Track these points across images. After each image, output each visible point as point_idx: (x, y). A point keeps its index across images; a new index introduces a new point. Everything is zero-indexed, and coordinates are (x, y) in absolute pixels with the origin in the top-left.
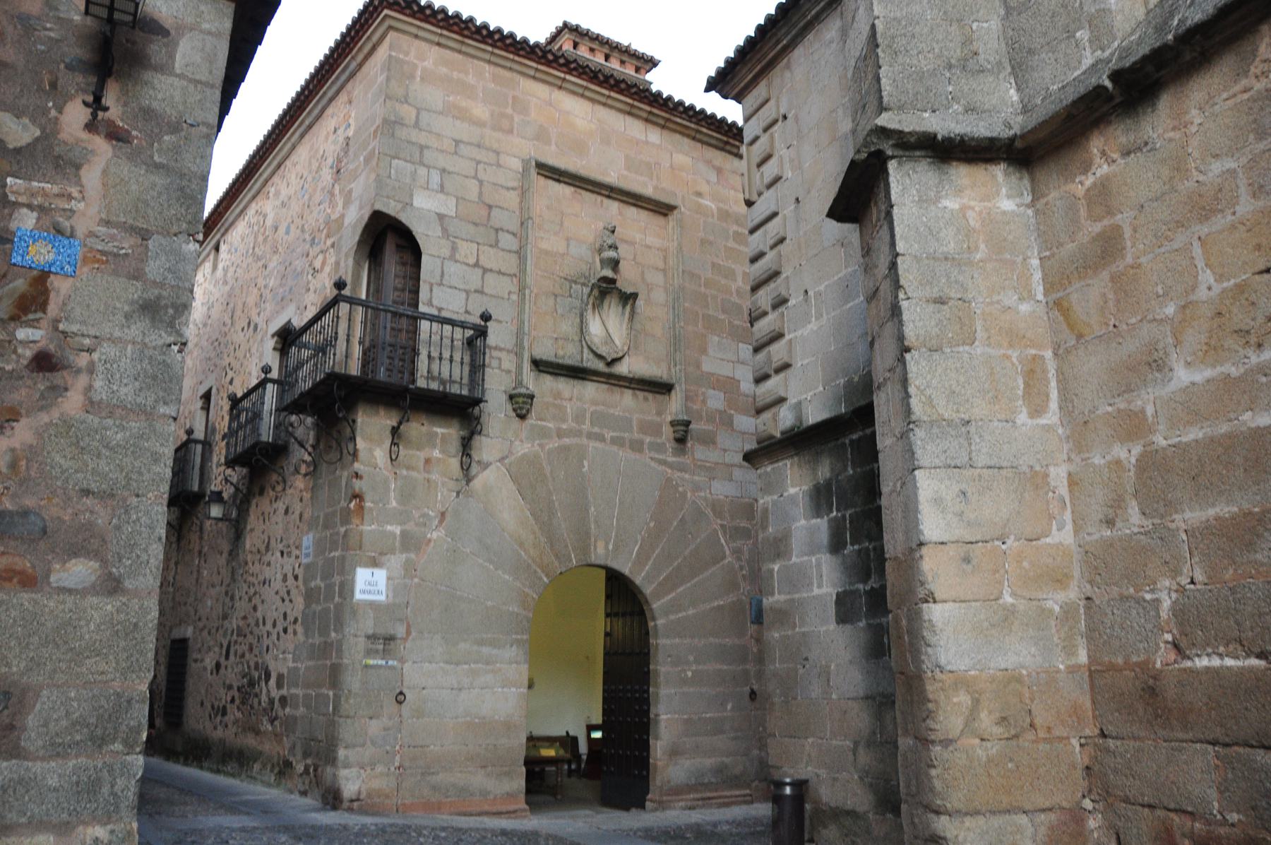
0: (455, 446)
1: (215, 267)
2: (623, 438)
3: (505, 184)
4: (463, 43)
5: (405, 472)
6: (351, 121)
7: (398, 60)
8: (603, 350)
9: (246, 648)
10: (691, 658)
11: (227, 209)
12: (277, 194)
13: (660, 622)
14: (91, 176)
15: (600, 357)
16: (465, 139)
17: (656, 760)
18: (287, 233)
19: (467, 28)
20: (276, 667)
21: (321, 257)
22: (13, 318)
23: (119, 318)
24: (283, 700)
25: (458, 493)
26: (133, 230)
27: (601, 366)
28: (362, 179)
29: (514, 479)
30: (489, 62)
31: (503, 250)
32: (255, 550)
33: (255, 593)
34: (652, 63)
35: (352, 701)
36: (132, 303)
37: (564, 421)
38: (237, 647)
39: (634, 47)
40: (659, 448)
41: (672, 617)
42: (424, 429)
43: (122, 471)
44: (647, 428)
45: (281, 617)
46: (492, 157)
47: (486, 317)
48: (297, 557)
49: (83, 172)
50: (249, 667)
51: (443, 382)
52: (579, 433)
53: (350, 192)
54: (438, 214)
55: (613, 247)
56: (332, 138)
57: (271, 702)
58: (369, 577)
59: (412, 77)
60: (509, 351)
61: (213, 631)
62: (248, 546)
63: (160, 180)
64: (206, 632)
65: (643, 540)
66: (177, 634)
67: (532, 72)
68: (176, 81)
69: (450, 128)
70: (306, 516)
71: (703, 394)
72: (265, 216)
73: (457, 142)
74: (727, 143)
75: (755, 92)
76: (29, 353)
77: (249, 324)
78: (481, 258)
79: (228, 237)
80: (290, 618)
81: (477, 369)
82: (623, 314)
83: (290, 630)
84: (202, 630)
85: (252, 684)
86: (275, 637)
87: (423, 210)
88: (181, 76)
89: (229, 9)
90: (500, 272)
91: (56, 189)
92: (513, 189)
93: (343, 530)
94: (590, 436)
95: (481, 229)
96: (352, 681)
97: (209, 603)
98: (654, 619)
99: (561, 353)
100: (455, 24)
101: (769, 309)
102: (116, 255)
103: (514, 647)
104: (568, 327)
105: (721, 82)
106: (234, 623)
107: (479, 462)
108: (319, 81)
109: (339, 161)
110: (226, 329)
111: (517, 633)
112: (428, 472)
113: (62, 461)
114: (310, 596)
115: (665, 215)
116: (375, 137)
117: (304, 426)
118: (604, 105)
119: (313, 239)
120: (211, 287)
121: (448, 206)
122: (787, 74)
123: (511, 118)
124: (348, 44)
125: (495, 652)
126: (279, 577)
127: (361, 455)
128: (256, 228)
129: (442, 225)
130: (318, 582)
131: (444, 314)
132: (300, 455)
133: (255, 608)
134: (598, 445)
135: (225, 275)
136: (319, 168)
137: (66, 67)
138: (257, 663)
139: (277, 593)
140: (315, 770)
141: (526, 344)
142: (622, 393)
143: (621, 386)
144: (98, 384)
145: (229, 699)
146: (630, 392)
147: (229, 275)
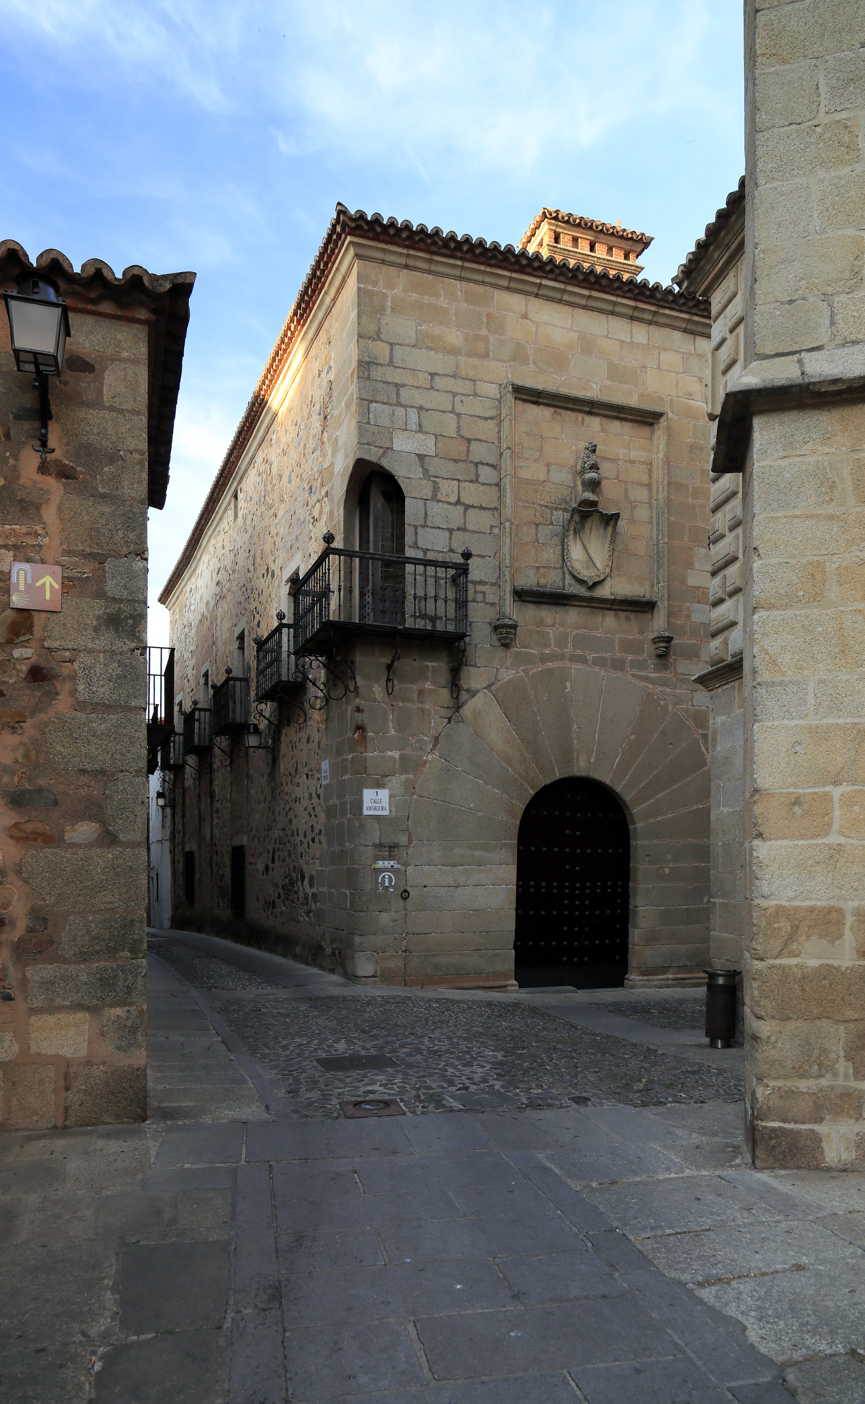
0: (444, 677)
1: (236, 516)
2: (606, 659)
4: (431, 261)
6: (332, 363)
9: (286, 854)
11: (238, 457)
12: (278, 441)
13: (640, 825)
14: (50, 514)
15: (581, 582)
16: (441, 372)
18: (290, 482)
19: (434, 243)
20: (308, 870)
21: (318, 506)
22: (10, 642)
23: (90, 632)
26: (92, 556)
28: (345, 425)
30: (461, 278)
31: (483, 484)
32: (287, 773)
33: (290, 809)
36: (98, 618)
37: (547, 646)
38: (280, 853)
40: (641, 665)
42: (416, 663)
43: (108, 753)
44: (627, 646)
45: (310, 830)
48: (318, 779)
49: (43, 511)
50: (289, 869)
52: (562, 657)
53: (336, 439)
54: (418, 455)
55: (594, 467)
56: (317, 381)
57: (306, 898)
58: (374, 797)
60: (493, 584)
61: (262, 839)
62: (282, 770)
64: (256, 840)
66: (236, 842)
67: (505, 283)
68: (107, 415)
69: (425, 360)
70: (322, 745)
72: (271, 464)
73: (433, 375)
76: (24, 668)
77: (268, 570)
78: (462, 494)
79: (243, 485)
80: (316, 831)
81: (462, 604)
83: (316, 840)
84: (253, 839)
85: (292, 883)
86: (306, 845)
87: (404, 453)
88: (112, 409)
90: (481, 508)
91: (24, 529)
92: (491, 418)
94: (573, 659)
95: (461, 465)
97: (257, 817)
98: (634, 823)
99: (543, 581)
102: (80, 579)
103: (503, 851)
104: (551, 554)
106: (276, 834)
107: (468, 690)
110: (250, 575)
111: (505, 839)
112: (422, 702)
113: (62, 750)
114: (330, 812)
115: (651, 424)
117: (317, 670)
118: (585, 307)
119: (311, 488)
120: (235, 535)
121: (428, 445)
123: (486, 340)
124: (320, 278)
125: (486, 854)
126: (307, 796)
127: (361, 691)
128: (264, 476)
130: (334, 801)
131: (431, 556)
132: (315, 693)
133: (290, 821)
134: (580, 666)
135: (245, 522)
137: (14, 418)
138: (294, 866)
139: (305, 809)
140: (340, 953)
142: (604, 615)
143: (603, 609)
144: (81, 687)
145: (276, 895)
146: (612, 613)
147: (248, 522)
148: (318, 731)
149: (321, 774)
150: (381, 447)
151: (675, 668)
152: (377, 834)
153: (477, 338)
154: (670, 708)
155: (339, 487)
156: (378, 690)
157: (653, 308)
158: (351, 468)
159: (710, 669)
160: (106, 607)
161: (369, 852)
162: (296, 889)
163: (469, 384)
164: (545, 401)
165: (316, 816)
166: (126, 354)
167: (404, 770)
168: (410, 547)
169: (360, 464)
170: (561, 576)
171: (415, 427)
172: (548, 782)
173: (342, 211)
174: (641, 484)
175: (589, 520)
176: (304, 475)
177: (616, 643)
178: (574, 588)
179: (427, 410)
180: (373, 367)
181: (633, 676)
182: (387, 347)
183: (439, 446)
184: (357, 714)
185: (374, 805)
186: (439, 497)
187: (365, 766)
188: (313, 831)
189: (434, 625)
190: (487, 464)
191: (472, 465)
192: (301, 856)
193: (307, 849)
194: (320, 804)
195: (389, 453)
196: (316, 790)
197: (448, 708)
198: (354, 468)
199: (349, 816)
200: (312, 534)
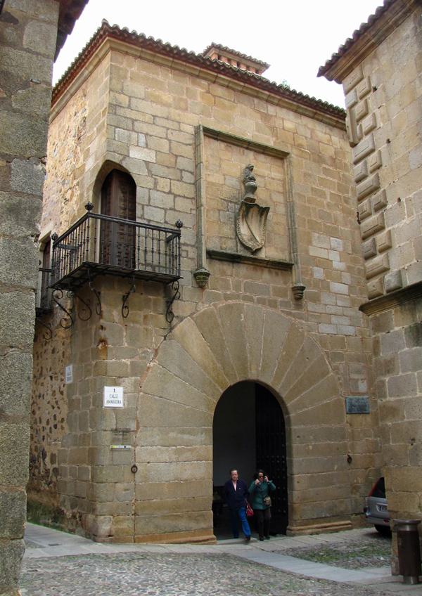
2: (265, 299)
3: (185, 142)
5: (132, 325)
6: (86, 107)
7: (116, 67)
8: (250, 244)
10: (311, 437)
15: (247, 248)
17: (292, 503)
21: (70, 192)
24: (55, 470)
25: (165, 337)
27: (248, 255)
28: (96, 142)
29: (200, 327)
31: (186, 183)
34: (265, 66)
35: (104, 472)
37: (228, 289)
39: (253, 57)
41: (299, 412)
42: (142, 297)
45: (52, 418)
46: (175, 126)
47: (179, 225)
48: (62, 380)
51: (151, 265)
52: (238, 297)
56: (73, 118)
58: (112, 393)
59: (125, 77)
63: (18, 120)
65: (279, 363)
68: (24, 53)
69: (150, 108)
71: (311, 269)
74: (316, 113)
75: (352, 75)
78: (172, 188)
80: (59, 419)
81: (174, 257)
82: (260, 221)
83: (59, 426)
86: (48, 431)
87: (137, 159)
88: (28, 50)
89: (56, 6)
90: (184, 197)
92: (190, 145)
93: (94, 363)
94: (246, 298)
95: (171, 170)
96: (105, 459)
100: (150, 44)
101: (373, 211)
104: (227, 230)
105: (331, 70)
108: (64, 84)
109: (80, 131)
111: (204, 426)
112: (146, 324)
114: (71, 404)
116: (104, 115)
117: (65, 298)
119: (64, 181)
121: (151, 156)
122: (375, 61)
123: (186, 102)
124: (83, 60)
125: (192, 437)
126: (50, 392)
127: (105, 314)
129: (147, 168)
130: (77, 396)
136: (66, 137)
138: (36, 447)
140: (80, 517)
141: (203, 242)
142: (262, 270)
143: (261, 266)
146: (267, 270)
148: (63, 344)
149: (64, 376)
150: (122, 155)
151: (307, 308)
152: (114, 421)
153: (181, 99)
154: (306, 334)
155: (90, 179)
156: (116, 314)
157: (279, 97)
158: (101, 166)
159: (368, 300)
160: (10, 198)
161: (108, 436)
162: (37, 464)
163: (176, 124)
164: (222, 139)
165: (59, 408)
166: (43, 17)
167: (134, 374)
168: (139, 218)
169: (108, 163)
170: (235, 243)
171: (143, 145)
172: (232, 384)
173: (105, 23)
174: (279, 192)
175: (252, 210)
176: (59, 174)
177: (271, 289)
178: (242, 252)
179: (151, 136)
180: (118, 108)
181: (282, 311)
182: (127, 99)
183: (158, 157)
184: (101, 331)
185: (112, 399)
186: (158, 188)
187: (106, 369)
188: (55, 419)
189: (154, 270)
190: (187, 171)
191: (178, 171)
192: (43, 439)
193: (49, 434)
194: (63, 399)
195: (127, 158)
196: (60, 388)
197: (164, 329)
198: (102, 166)
199: (91, 407)
200: (64, 210)
